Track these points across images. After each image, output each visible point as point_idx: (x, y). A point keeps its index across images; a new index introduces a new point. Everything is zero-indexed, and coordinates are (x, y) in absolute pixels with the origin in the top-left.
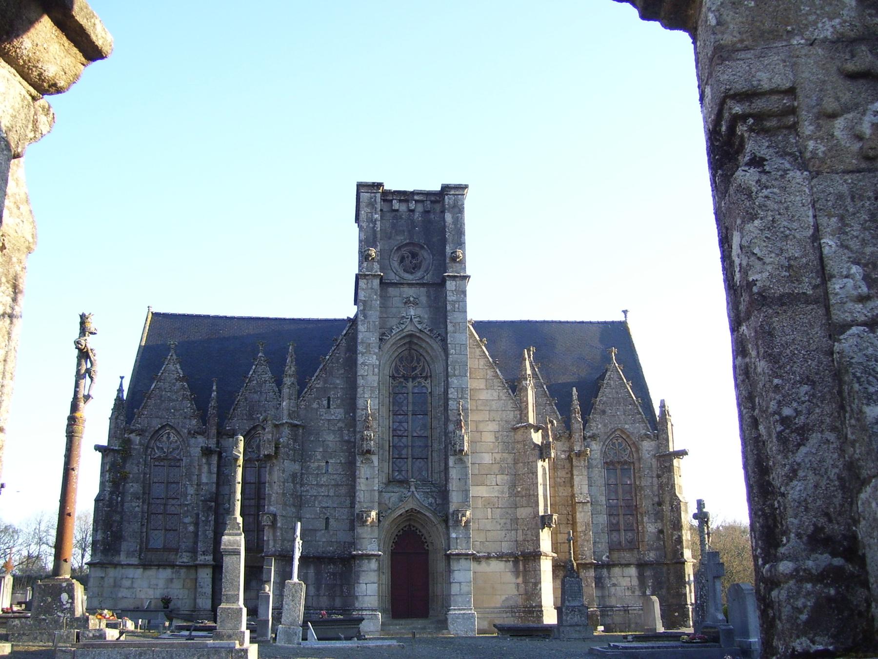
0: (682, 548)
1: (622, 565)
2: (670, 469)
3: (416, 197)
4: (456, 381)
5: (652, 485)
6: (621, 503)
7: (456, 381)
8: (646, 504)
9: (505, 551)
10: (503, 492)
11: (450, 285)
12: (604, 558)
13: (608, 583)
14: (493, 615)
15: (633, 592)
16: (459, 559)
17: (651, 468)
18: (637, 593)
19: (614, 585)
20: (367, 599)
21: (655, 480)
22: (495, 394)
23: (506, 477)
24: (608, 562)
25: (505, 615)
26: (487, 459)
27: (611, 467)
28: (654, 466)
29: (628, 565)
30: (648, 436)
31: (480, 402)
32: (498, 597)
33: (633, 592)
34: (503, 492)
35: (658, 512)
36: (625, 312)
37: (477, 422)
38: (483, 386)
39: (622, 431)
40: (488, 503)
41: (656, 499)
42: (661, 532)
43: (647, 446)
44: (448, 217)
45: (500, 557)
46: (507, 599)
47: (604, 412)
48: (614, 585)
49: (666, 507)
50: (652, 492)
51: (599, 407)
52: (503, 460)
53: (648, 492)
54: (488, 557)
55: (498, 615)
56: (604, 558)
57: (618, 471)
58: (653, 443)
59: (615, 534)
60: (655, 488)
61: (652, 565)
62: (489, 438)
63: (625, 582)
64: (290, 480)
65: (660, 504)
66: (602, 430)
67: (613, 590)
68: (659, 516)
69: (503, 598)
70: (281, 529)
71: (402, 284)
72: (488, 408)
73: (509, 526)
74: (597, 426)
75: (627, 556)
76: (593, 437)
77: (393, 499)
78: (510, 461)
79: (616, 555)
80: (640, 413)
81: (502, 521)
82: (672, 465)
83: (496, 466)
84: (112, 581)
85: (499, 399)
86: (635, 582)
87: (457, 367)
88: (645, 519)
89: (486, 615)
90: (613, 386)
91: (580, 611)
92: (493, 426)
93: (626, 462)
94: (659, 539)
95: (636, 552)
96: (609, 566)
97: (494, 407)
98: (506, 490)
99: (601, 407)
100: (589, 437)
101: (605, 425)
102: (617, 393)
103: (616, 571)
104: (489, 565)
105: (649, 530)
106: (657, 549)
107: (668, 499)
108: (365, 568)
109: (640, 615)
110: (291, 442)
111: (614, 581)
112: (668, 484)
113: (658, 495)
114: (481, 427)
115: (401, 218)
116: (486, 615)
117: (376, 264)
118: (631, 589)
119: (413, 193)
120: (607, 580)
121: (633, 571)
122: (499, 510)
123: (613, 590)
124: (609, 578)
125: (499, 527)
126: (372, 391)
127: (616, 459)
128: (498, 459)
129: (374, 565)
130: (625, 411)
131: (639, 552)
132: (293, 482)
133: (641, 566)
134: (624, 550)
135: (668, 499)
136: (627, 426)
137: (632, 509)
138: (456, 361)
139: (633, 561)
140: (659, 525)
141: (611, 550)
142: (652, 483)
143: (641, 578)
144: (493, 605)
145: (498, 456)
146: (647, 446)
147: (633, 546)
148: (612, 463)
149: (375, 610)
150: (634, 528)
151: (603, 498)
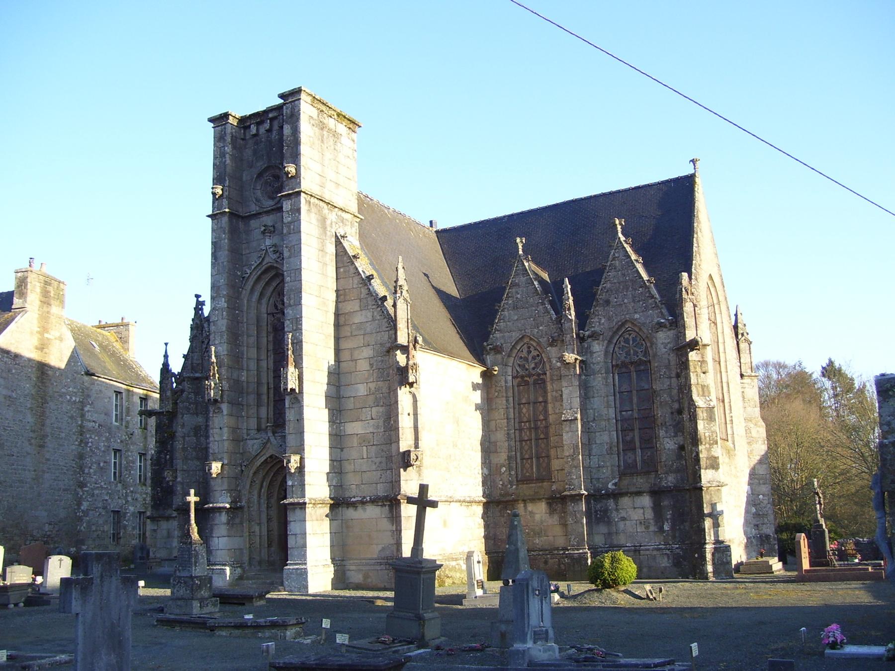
0: (700, 468)
1: (632, 493)
2: (684, 365)
3: (270, 115)
4: (291, 312)
5: (670, 387)
6: (636, 415)
7: (291, 312)
8: (662, 413)
9: (381, 494)
10: (378, 427)
11: (287, 205)
12: (610, 486)
13: (615, 517)
14: (368, 568)
15: (647, 527)
16: (294, 509)
17: (668, 367)
18: (652, 528)
19: (623, 519)
20: (219, 552)
21: (674, 380)
22: (369, 315)
23: (381, 409)
24: (613, 490)
25: (378, 568)
26: (362, 390)
27: (624, 370)
28: (673, 363)
29: (639, 493)
30: (661, 325)
31: (354, 327)
32: (374, 546)
33: (647, 527)
34: (378, 427)
35: (679, 423)
36: (693, 161)
37: (352, 350)
38: (357, 308)
39: (633, 322)
40: (363, 440)
41: (676, 406)
42: (682, 448)
43: (663, 337)
44: (287, 130)
45: (374, 501)
46: (383, 549)
47: (607, 302)
48: (623, 519)
49: (686, 416)
50: (671, 397)
51: (601, 296)
52: (378, 389)
53: (665, 397)
54: (363, 503)
55: (372, 567)
56: (610, 486)
57: (634, 375)
58: (671, 333)
59: (630, 454)
60: (675, 392)
61: (671, 491)
62: (363, 365)
63: (637, 515)
64: (192, 434)
65: (680, 412)
66: (606, 326)
67: (621, 525)
68: (678, 428)
69: (380, 547)
70: (182, 483)
71: (260, 214)
72: (362, 332)
73: (384, 465)
74: (599, 322)
75: (640, 482)
76: (594, 336)
77: (255, 447)
78: (385, 390)
79: (626, 481)
80: (652, 297)
81: (379, 460)
82: (687, 360)
83: (371, 398)
84: (165, 532)
85: (374, 320)
86: (649, 514)
87: (292, 296)
88: (662, 433)
89: (361, 567)
90: (619, 267)
91: (185, 583)
92: (367, 352)
93: (641, 362)
94: (680, 457)
95: (653, 475)
96: (616, 495)
97: (368, 330)
98: (381, 424)
99: (604, 296)
100: (589, 337)
101: (609, 319)
102: (624, 275)
103: (625, 501)
104: (365, 510)
105: (667, 446)
106: (677, 471)
107: (686, 405)
108: (217, 522)
109: (654, 557)
110: (192, 396)
111: (623, 514)
112: (685, 385)
113: (679, 401)
114: (356, 355)
115: (261, 142)
116: (361, 567)
117: (225, 200)
118: (644, 523)
119: (266, 112)
120: (614, 514)
121: (646, 501)
122: (374, 447)
123: (621, 525)
124: (617, 510)
125: (374, 467)
126: (222, 336)
127: (627, 360)
128: (373, 389)
129: (224, 518)
130: (634, 297)
131: (657, 476)
132: (196, 435)
133: (656, 493)
134: (638, 474)
135: (686, 405)
136: (637, 316)
137: (648, 422)
138: (291, 290)
139: (646, 487)
140: (680, 440)
141: (622, 475)
142: (670, 385)
143: (657, 509)
144: (370, 556)
145: (372, 386)
146: (663, 337)
147: (651, 466)
148: (624, 365)
149: (225, 565)
150: (649, 443)
151: (612, 411)
